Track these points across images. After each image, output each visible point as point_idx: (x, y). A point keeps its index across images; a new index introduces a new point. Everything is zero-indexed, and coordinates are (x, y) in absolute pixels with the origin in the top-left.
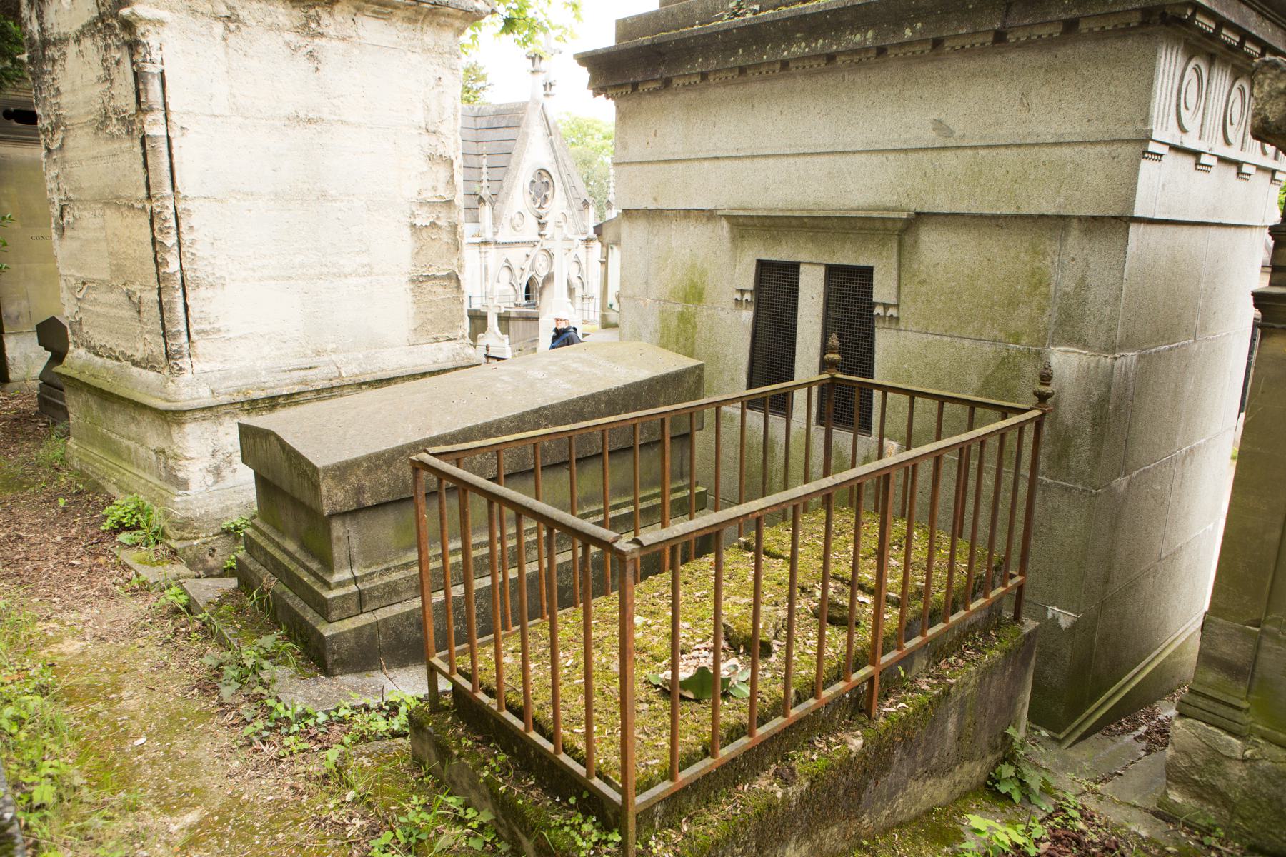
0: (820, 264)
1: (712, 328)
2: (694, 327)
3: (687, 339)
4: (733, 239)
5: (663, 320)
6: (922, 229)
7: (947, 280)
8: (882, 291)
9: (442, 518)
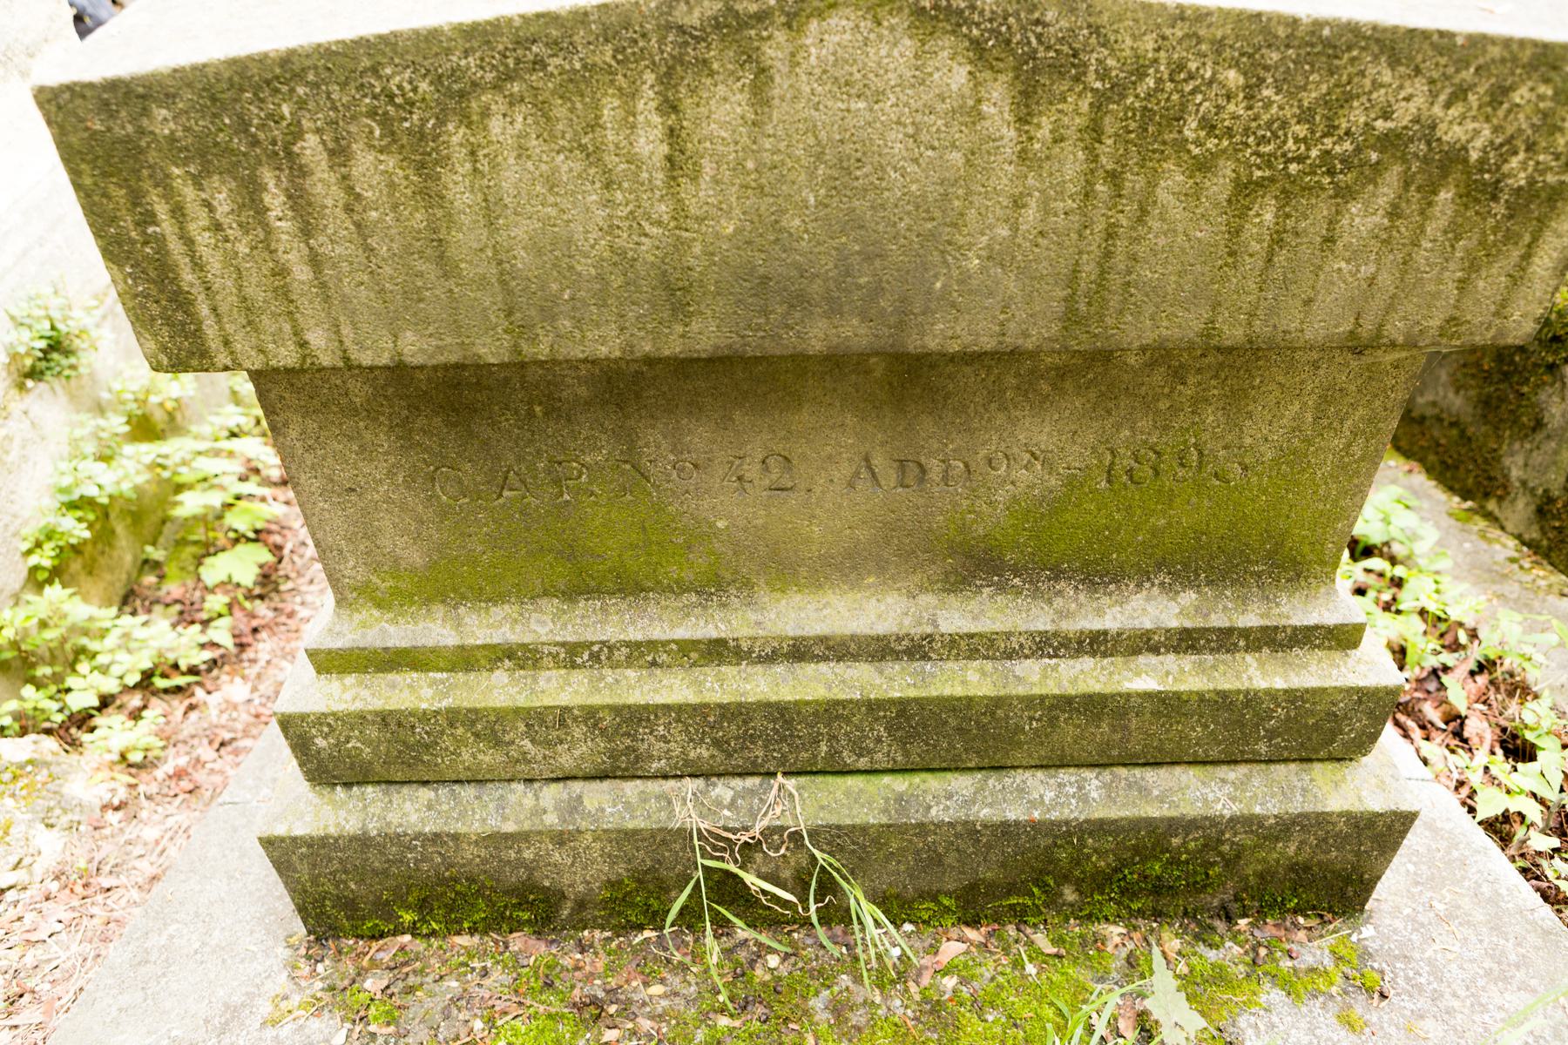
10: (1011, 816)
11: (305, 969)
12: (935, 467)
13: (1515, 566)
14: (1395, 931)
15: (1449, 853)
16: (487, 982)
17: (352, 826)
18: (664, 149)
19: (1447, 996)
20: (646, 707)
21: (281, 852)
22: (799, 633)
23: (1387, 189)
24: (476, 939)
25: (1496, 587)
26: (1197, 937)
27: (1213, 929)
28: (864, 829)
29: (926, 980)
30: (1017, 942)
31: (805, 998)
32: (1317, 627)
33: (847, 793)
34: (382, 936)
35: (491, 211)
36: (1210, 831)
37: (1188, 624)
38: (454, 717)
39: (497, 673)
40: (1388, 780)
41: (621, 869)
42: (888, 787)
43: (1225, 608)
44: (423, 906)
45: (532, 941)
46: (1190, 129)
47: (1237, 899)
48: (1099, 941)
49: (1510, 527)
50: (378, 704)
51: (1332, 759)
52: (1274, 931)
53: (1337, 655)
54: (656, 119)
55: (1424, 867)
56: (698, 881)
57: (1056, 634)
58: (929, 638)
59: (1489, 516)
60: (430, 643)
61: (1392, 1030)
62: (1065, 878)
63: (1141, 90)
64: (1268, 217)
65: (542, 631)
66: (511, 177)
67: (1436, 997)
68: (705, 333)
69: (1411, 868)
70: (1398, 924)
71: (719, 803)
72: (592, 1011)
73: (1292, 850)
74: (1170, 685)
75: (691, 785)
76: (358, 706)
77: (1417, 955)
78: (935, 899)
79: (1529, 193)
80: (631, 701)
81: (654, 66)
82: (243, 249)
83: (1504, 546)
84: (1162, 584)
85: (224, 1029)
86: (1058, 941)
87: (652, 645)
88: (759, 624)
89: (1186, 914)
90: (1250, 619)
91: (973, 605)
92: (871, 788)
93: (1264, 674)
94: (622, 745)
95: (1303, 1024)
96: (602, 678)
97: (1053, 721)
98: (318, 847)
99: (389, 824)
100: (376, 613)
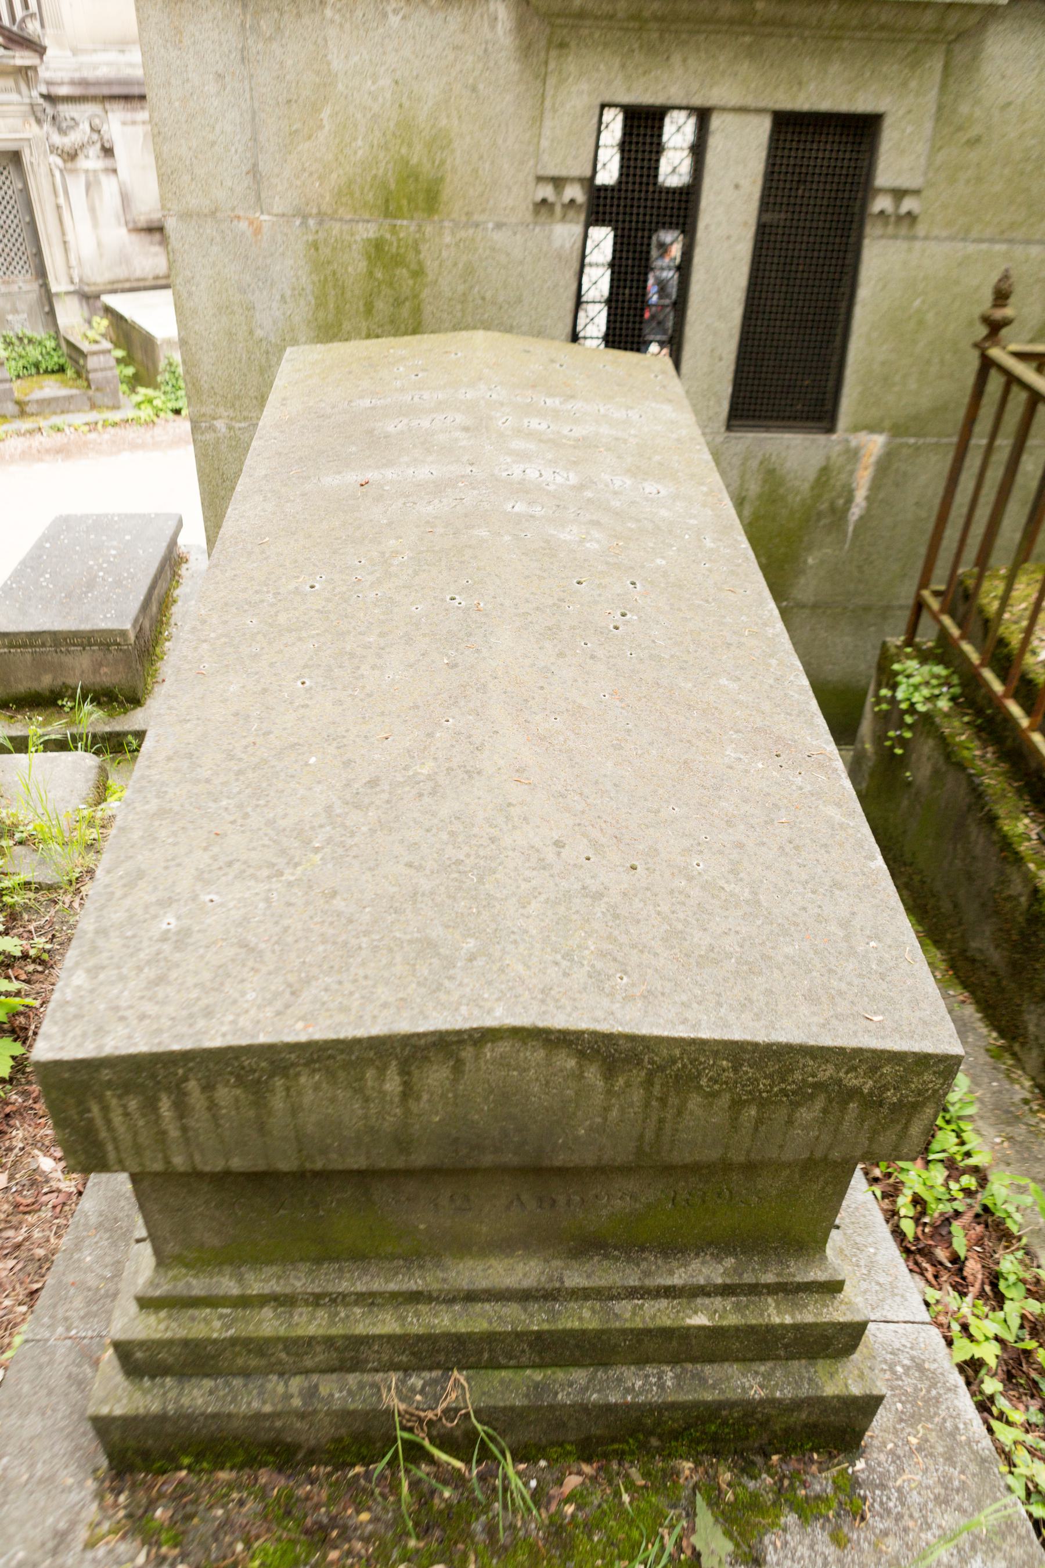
0: (759, 111)
1: (469, 270)
2: (418, 273)
3: (398, 303)
4: (526, 50)
5: (317, 266)
6: (989, 42)
7: (1021, 136)
8: (895, 163)
9: (923, 1323)
10: (612, 1400)
11: (110, 1498)
12: (562, 1200)
13: (1026, 1108)
14: (879, 1464)
15: (928, 1392)
16: (245, 1510)
17: (155, 1407)
18: (400, 1089)
19: (906, 1517)
20: (367, 1336)
21: (102, 1426)
22: (471, 1287)
23: (819, 1103)
24: (234, 1474)
25: (1009, 1129)
26: (743, 1470)
27: (753, 1463)
28: (512, 1408)
29: (553, 1508)
30: (618, 1474)
31: (469, 1524)
32: (813, 1282)
33: (502, 1382)
34: (165, 1472)
35: (294, 1111)
36: (749, 1409)
37: (728, 1281)
38: (234, 1341)
39: (265, 1309)
40: (866, 1371)
41: (343, 1431)
42: (529, 1377)
43: (753, 1269)
44: (199, 1457)
45: (275, 1475)
46: (704, 1082)
47: (770, 1443)
48: (676, 1473)
49: (1028, 1067)
50: (181, 1333)
51: (828, 1357)
52: (796, 1465)
53: (828, 1298)
54: (397, 1078)
55: (909, 1406)
56: (396, 1451)
57: (641, 1288)
58: (559, 1290)
59: (1014, 1055)
60: (221, 1293)
61: (866, 1546)
62: (651, 1433)
63: (675, 1068)
64: (753, 1113)
65: (298, 1284)
66: (308, 1098)
67: (899, 1517)
68: (420, 1159)
69: (899, 1406)
70: (882, 1457)
71: (413, 1390)
72: (319, 1536)
73: (804, 1416)
74: (717, 1321)
75: (394, 1377)
76: (168, 1335)
77: (891, 1484)
78: (561, 1445)
79: (895, 1108)
80: (357, 1332)
81: (397, 1058)
82: (141, 1123)
83: (1022, 1087)
84: (712, 1254)
85: (55, 1552)
86: (646, 1475)
87: (372, 1294)
88: (444, 1280)
89: (736, 1452)
90: (769, 1278)
91: (587, 1267)
92: (518, 1379)
93: (779, 1313)
94: (350, 1355)
95: (807, 1542)
96: (337, 1314)
97: (640, 1342)
98: (128, 1422)
99: (182, 1406)
100: (184, 1271)
